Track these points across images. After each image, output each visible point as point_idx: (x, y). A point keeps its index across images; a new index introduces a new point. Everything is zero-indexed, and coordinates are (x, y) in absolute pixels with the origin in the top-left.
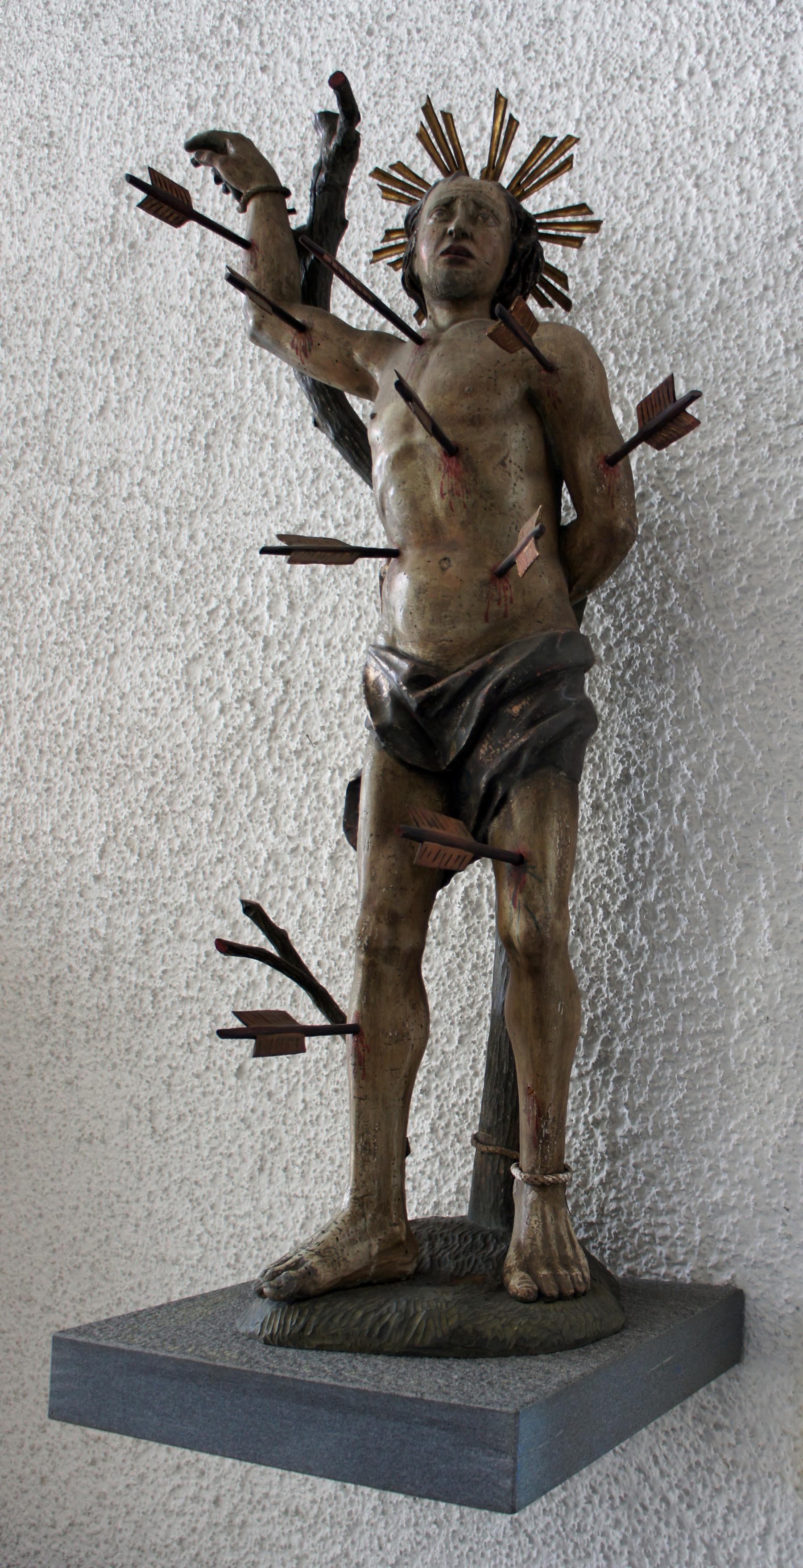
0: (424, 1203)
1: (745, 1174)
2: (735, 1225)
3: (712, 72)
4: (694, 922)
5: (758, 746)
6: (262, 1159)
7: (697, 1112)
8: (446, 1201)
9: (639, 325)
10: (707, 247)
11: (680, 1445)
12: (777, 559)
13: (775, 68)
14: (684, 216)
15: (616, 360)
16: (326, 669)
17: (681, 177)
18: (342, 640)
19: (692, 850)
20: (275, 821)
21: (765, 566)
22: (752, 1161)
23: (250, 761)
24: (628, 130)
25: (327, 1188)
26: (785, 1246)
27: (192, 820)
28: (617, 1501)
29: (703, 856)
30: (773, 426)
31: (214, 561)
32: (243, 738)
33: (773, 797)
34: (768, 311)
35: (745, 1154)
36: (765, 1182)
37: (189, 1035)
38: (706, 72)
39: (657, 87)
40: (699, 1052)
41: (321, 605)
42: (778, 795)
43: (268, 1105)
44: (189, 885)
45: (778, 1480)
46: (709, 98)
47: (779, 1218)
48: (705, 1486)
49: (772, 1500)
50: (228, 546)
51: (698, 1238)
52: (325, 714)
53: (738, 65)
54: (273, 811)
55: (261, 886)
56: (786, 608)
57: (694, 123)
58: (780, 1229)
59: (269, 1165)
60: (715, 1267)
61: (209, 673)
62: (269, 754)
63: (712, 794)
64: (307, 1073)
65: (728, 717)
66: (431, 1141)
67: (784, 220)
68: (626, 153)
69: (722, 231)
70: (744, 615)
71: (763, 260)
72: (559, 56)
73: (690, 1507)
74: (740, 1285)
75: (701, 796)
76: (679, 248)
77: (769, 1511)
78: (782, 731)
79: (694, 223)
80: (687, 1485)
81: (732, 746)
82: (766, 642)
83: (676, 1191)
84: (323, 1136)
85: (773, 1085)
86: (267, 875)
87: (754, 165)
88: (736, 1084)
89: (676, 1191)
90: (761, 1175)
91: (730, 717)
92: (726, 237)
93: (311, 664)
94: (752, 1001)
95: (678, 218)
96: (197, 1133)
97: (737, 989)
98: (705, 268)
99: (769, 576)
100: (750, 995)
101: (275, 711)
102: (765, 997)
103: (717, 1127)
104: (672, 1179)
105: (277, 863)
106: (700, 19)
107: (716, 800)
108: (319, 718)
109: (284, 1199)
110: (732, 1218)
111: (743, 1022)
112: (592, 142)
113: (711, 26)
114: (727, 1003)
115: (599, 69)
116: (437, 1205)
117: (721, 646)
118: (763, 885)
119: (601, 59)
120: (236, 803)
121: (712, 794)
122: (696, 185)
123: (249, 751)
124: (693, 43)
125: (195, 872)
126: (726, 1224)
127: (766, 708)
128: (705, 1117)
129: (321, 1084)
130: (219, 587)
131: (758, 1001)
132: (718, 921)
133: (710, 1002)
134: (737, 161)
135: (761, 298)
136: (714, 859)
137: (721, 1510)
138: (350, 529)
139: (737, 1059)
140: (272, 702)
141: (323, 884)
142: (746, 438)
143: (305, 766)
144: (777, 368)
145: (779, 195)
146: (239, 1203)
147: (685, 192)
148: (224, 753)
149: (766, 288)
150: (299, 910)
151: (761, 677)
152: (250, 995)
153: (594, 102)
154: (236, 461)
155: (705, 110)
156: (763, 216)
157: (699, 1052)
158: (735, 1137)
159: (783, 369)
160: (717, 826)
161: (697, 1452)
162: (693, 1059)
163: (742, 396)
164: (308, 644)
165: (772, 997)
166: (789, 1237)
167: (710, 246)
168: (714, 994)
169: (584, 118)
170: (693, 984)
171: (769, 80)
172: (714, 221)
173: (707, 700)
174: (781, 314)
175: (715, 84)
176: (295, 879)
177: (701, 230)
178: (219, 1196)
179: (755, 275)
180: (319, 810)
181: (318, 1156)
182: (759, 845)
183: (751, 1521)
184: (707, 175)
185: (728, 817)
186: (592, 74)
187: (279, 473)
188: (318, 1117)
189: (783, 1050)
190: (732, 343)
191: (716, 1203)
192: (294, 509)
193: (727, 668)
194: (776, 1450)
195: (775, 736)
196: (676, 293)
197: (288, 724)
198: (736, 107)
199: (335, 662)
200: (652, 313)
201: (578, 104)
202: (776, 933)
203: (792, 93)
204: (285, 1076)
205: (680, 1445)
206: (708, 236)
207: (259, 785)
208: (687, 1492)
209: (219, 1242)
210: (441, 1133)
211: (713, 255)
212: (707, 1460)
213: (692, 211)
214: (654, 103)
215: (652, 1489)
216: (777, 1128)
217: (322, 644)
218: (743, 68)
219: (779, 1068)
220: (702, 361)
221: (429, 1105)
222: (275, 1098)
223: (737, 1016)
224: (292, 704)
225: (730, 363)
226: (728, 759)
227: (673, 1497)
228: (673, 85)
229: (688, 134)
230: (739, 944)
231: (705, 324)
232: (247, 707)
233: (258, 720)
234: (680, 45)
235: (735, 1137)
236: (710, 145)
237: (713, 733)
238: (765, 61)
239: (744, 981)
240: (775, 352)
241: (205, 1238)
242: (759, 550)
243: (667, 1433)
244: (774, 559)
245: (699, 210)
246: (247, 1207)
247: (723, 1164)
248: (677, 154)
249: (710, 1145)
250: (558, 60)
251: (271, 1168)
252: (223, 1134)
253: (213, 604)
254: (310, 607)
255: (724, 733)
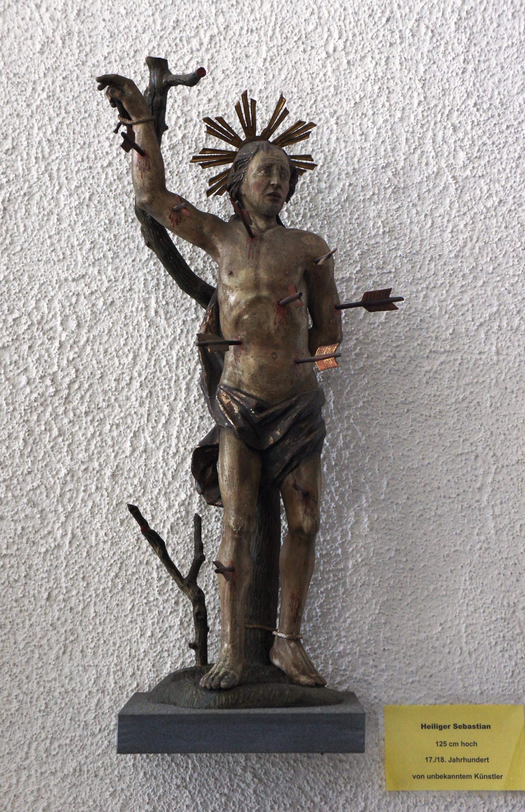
0: (176, 662)
1: (354, 637)
2: (349, 662)
3: (347, 54)
4: (329, 516)
5: (363, 433)
6: (65, 646)
7: (330, 609)
8: (189, 661)
9: (302, 199)
10: (341, 162)
11: (320, 773)
12: (375, 341)
13: (383, 62)
14: (329, 140)
15: (289, 217)
16: (105, 366)
17: (327, 114)
18: (116, 350)
19: (328, 481)
20: (70, 451)
21: (369, 344)
22: (358, 631)
23: (51, 415)
24: (296, 75)
25: (111, 660)
26: (373, 671)
27: (7, 448)
28: (288, 806)
29: (334, 485)
30: (374, 271)
31: (15, 287)
32: (45, 400)
33: (370, 458)
34: (374, 207)
35: (354, 628)
36: (364, 641)
37: (8, 577)
38: (343, 53)
39: (314, 52)
40: (331, 580)
41: (100, 327)
42: (373, 457)
43: (69, 615)
44: (7, 487)
45: (370, 783)
46: (345, 70)
47: (371, 658)
48: (333, 792)
49: (367, 793)
50: (26, 278)
51: (330, 670)
52: (105, 392)
53: (363, 55)
54: (69, 446)
55: (62, 489)
56: (379, 366)
57: (335, 83)
58: (371, 663)
59: (69, 649)
60: (340, 683)
61: (16, 357)
62: (65, 412)
63: (339, 455)
64: (97, 596)
65: (348, 418)
66: (180, 629)
67: (385, 157)
68: (295, 90)
69: (350, 155)
70: (357, 367)
71: (372, 177)
72: (252, 10)
73: (326, 803)
74: (351, 690)
75: (334, 455)
76: (325, 159)
77: (366, 799)
78: (375, 427)
79: (335, 146)
80: (324, 793)
81: (350, 432)
82: (369, 382)
83: (319, 647)
84: (108, 631)
85: (368, 595)
86: (65, 483)
87: (369, 119)
88: (350, 595)
89: (319, 647)
90: (362, 638)
91: (349, 418)
92: (352, 159)
93: (94, 362)
94: (358, 555)
95: (325, 140)
96: (14, 634)
97: (350, 550)
98: (340, 174)
99: (371, 350)
100: (357, 553)
101: (69, 387)
102: (364, 554)
103: (340, 616)
104: (317, 642)
105: (73, 476)
106: (340, 16)
107: (341, 457)
108: (101, 394)
109: (81, 668)
110: (347, 659)
111: (354, 565)
112: (274, 77)
113: (347, 22)
114: (346, 556)
115: (278, 29)
116: (183, 663)
117: (344, 381)
118: (364, 501)
119: (279, 21)
120: (41, 440)
121: (339, 455)
122: (337, 123)
123: (50, 409)
124: (337, 32)
125: (11, 479)
126: (344, 663)
127: (367, 415)
128: (334, 611)
129: (107, 602)
130: (21, 304)
131: (361, 555)
132: (341, 517)
133: (337, 555)
134: (360, 114)
135: (370, 199)
136: (340, 487)
137: (342, 802)
138: (118, 283)
139: (351, 582)
140: (67, 380)
141: (107, 490)
142: (360, 275)
143: (92, 421)
144: (377, 240)
145: (382, 142)
146: (47, 673)
147: (329, 125)
148: (31, 409)
149: (374, 194)
150: (90, 504)
151: (365, 400)
152: (55, 552)
153: (275, 50)
154: (29, 223)
155: (342, 77)
156: (373, 152)
157: (331, 580)
158: (349, 621)
159: (381, 241)
160: (341, 470)
161: (330, 775)
162: (327, 584)
163: (359, 252)
164: (92, 349)
165: (368, 553)
166: (376, 666)
167: (343, 162)
168: (340, 551)
169: (269, 59)
170: (328, 547)
171: (379, 69)
172: (346, 147)
173: (337, 408)
174: (381, 211)
175: (348, 62)
176: (86, 486)
177: (338, 151)
178: (32, 671)
179: (368, 185)
180: (103, 447)
181: (105, 642)
182: (363, 481)
183: (357, 806)
184: (343, 118)
185: (347, 467)
186: (274, 30)
187: (63, 239)
188: (105, 620)
189: (373, 578)
190: (354, 221)
191: (340, 652)
192: (76, 265)
193: (348, 393)
194: (369, 769)
195: (371, 429)
196: (323, 185)
197: (79, 396)
198: (360, 80)
199: (111, 362)
200: (309, 193)
201: (264, 48)
202: (371, 523)
203: (392, 81)
204: (81, 598)
205: (320, 773)
206: (342, 156)
207: (59, 430)
208: (324, 796)
209: (31, 698)
210: (186, 624)
211: (344, 167)
212: (335, 778)
213: (334, 138)
214: (311, 62)
215: (306, 797)
216: (370, 615)
217: (102, 350)
218: (365, 57)
219: (371, 587)
220: (337, 228)
221: (178, 610)
222: (75, 611)
223: (350, 564)
224: (81, 384)
225: (352, 232)
226: (348, 438)
227: (317, 800)
228: (324, 55)
229: (332, 89)
230: (352, 528)
231: (340, 207)
232: (48, 382)
233: (57, 392)
234: (329, 30)
235: (349, 621)
236: (345, 100)
237: (340, 425)
238: (378, 57)
239: (354, 545)
240: (378, 231)
241: (21, 697)
242: (365, 335)
243: (314, 768)
244: (373, 341)
245: (337, 139)
246: (53, 675)
247: (343, 634)
248: (326, 100)
249: (337, 625)
250: (251, 13)
251: (71, 651)
252: (35, 634)
253: (16, 314)
254: (92, 327)
255: (346, 426)
